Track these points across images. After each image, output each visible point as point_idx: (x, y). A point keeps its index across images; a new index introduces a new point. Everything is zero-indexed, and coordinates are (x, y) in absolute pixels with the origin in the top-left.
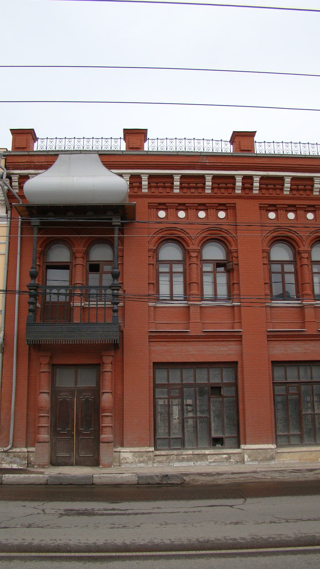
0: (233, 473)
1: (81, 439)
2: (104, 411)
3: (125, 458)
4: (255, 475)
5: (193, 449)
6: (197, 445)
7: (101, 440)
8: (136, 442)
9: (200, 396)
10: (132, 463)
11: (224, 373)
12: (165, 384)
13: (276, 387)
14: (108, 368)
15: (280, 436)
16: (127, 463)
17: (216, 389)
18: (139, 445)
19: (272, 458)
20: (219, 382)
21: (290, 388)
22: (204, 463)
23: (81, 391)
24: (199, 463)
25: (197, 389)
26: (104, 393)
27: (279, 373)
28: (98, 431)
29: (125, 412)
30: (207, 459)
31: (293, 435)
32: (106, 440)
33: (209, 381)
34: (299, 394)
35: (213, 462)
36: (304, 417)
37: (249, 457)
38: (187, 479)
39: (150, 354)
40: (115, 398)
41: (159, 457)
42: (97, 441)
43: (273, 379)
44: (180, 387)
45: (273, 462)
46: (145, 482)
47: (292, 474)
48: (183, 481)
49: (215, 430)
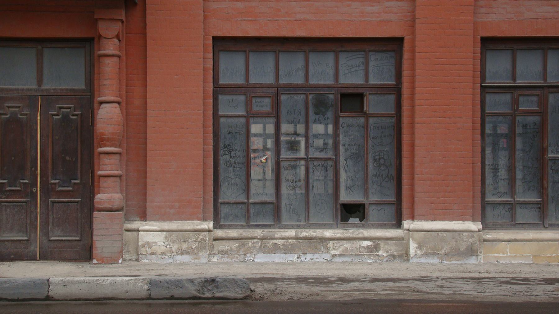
0: (374, 280)
1: (53, 202)
2: (103, 142)
3: (148, 243)
4: (421, 286)
5: (299, 227)
6: (307, 218)
7: (96, 205)
8: (172, 211)
9: (316, 113)
10: (164, 254)
11: (371, 63)
12: (239, 86)
13: (488, 98)
14: (110, 47)
15: (494, 204)
16: (152, 254)
17: (352, 100)
18: (180, 216)
19: (471, 251)
20: (361, 82)
21: (521, 99)
22: (320, 257)
23: (50, 99)
24: (309, 256)
25: (310, 97)
26: (101, 103)
27: (499, 67)
28: (89, 188)
29: (149, 146)
30: (328, 249)
31: (524, 204)
32: (106, 205)
33: (337, 80)
34: (542, 113)
35: (340, 255)
36: (550, 163)
37: (420, 247)
38: (260, 289)
39: (206, 18)
40: (127, 115)
41: (224, 242)
42: (89, 208)
43: (483, 78)
44: (272, 91)
45: (472, 261)
46: (164, 293)
47: (505, 287)
48: (248, 293)
49: (348, 188)
